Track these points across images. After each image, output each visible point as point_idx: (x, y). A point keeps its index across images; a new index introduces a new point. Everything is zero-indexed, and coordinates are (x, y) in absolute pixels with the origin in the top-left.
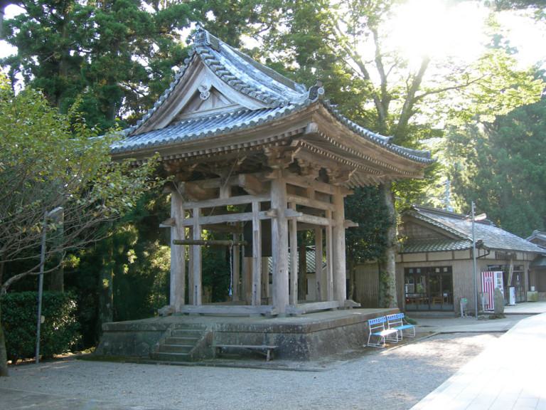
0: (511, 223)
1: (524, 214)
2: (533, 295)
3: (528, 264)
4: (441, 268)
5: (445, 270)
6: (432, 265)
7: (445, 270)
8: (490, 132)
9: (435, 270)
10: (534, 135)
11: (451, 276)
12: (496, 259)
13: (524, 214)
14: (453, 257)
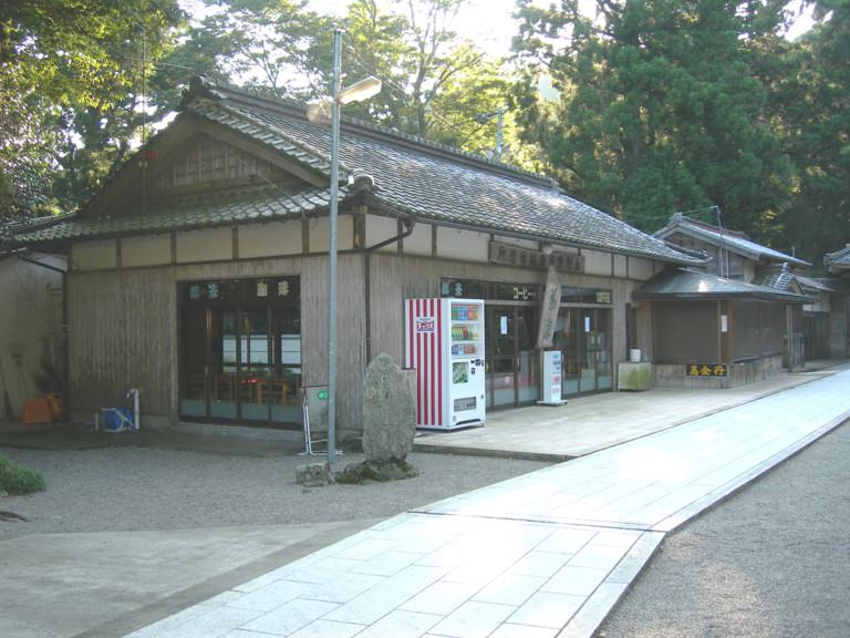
0: (639, 206)
1: (669, 187)
2: (634, 373)
3: (630, 288)
4: (273, 282)
5: (283, 289)
6: (247, 271)
7: (283, 289)
8: (607, 13)
9: (255, 289)
10: (703, 20)
11: (298, 302)
12: (491, 264)
13: (669, 187)
14: (306, 246)
